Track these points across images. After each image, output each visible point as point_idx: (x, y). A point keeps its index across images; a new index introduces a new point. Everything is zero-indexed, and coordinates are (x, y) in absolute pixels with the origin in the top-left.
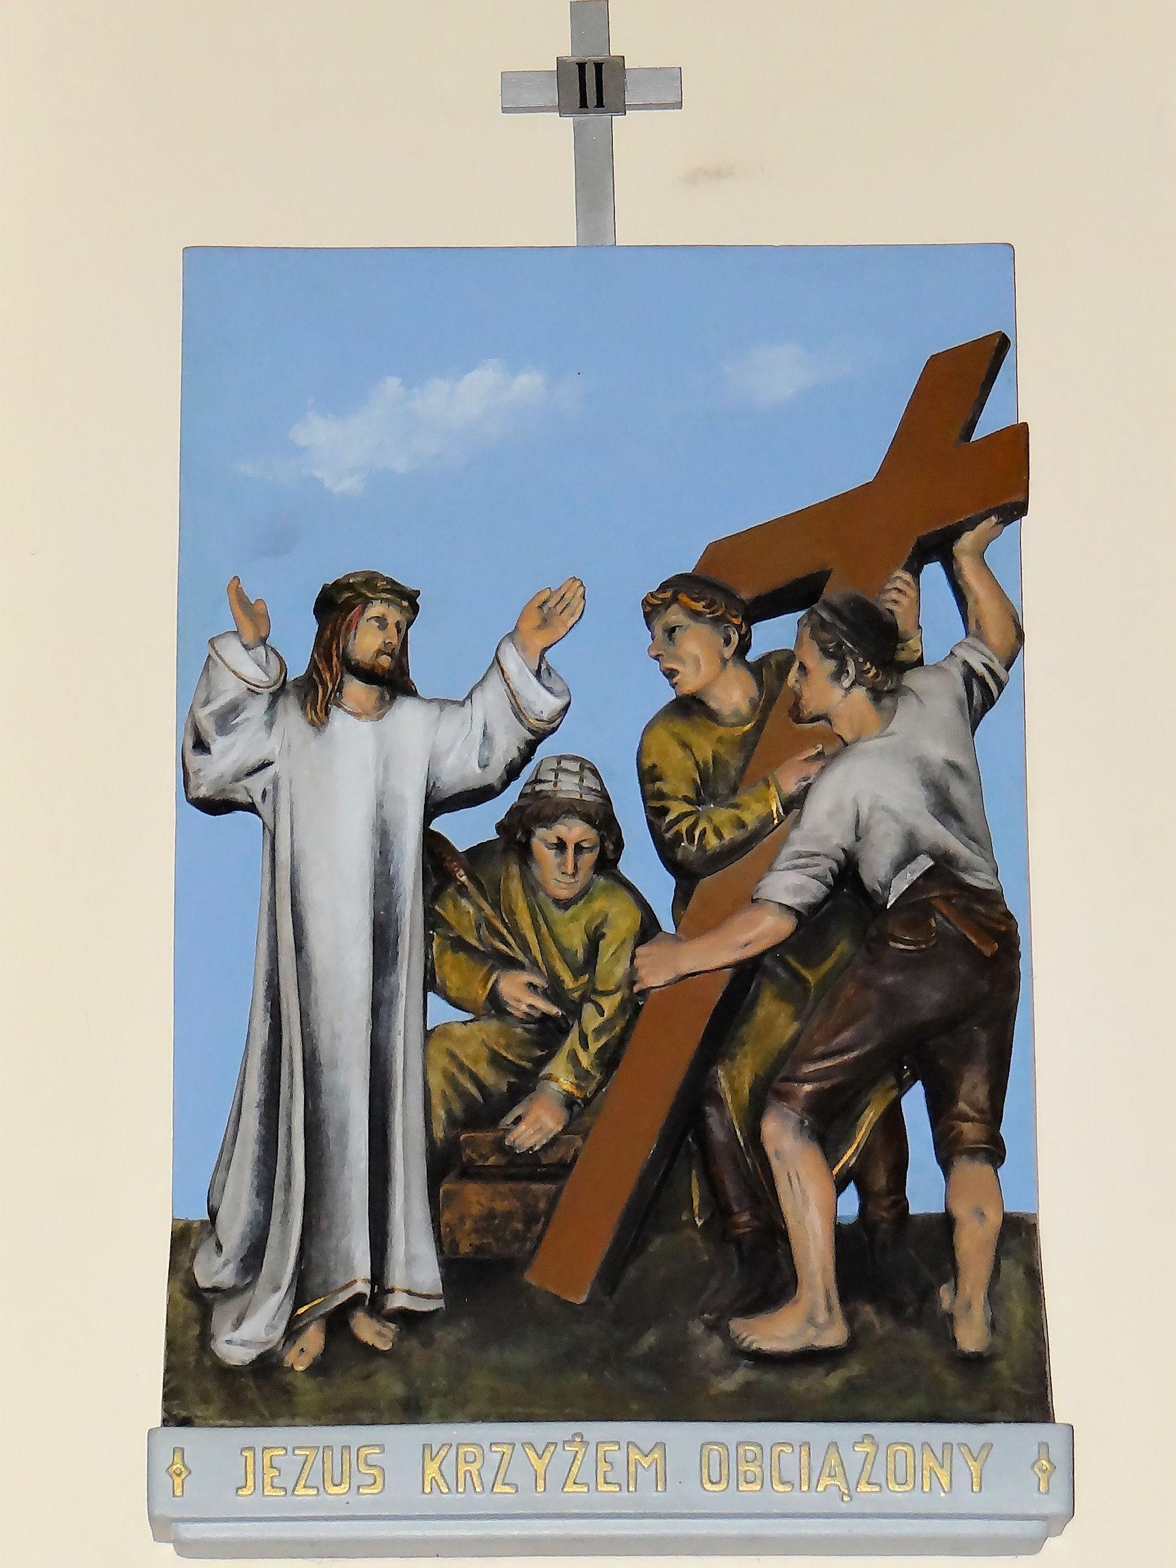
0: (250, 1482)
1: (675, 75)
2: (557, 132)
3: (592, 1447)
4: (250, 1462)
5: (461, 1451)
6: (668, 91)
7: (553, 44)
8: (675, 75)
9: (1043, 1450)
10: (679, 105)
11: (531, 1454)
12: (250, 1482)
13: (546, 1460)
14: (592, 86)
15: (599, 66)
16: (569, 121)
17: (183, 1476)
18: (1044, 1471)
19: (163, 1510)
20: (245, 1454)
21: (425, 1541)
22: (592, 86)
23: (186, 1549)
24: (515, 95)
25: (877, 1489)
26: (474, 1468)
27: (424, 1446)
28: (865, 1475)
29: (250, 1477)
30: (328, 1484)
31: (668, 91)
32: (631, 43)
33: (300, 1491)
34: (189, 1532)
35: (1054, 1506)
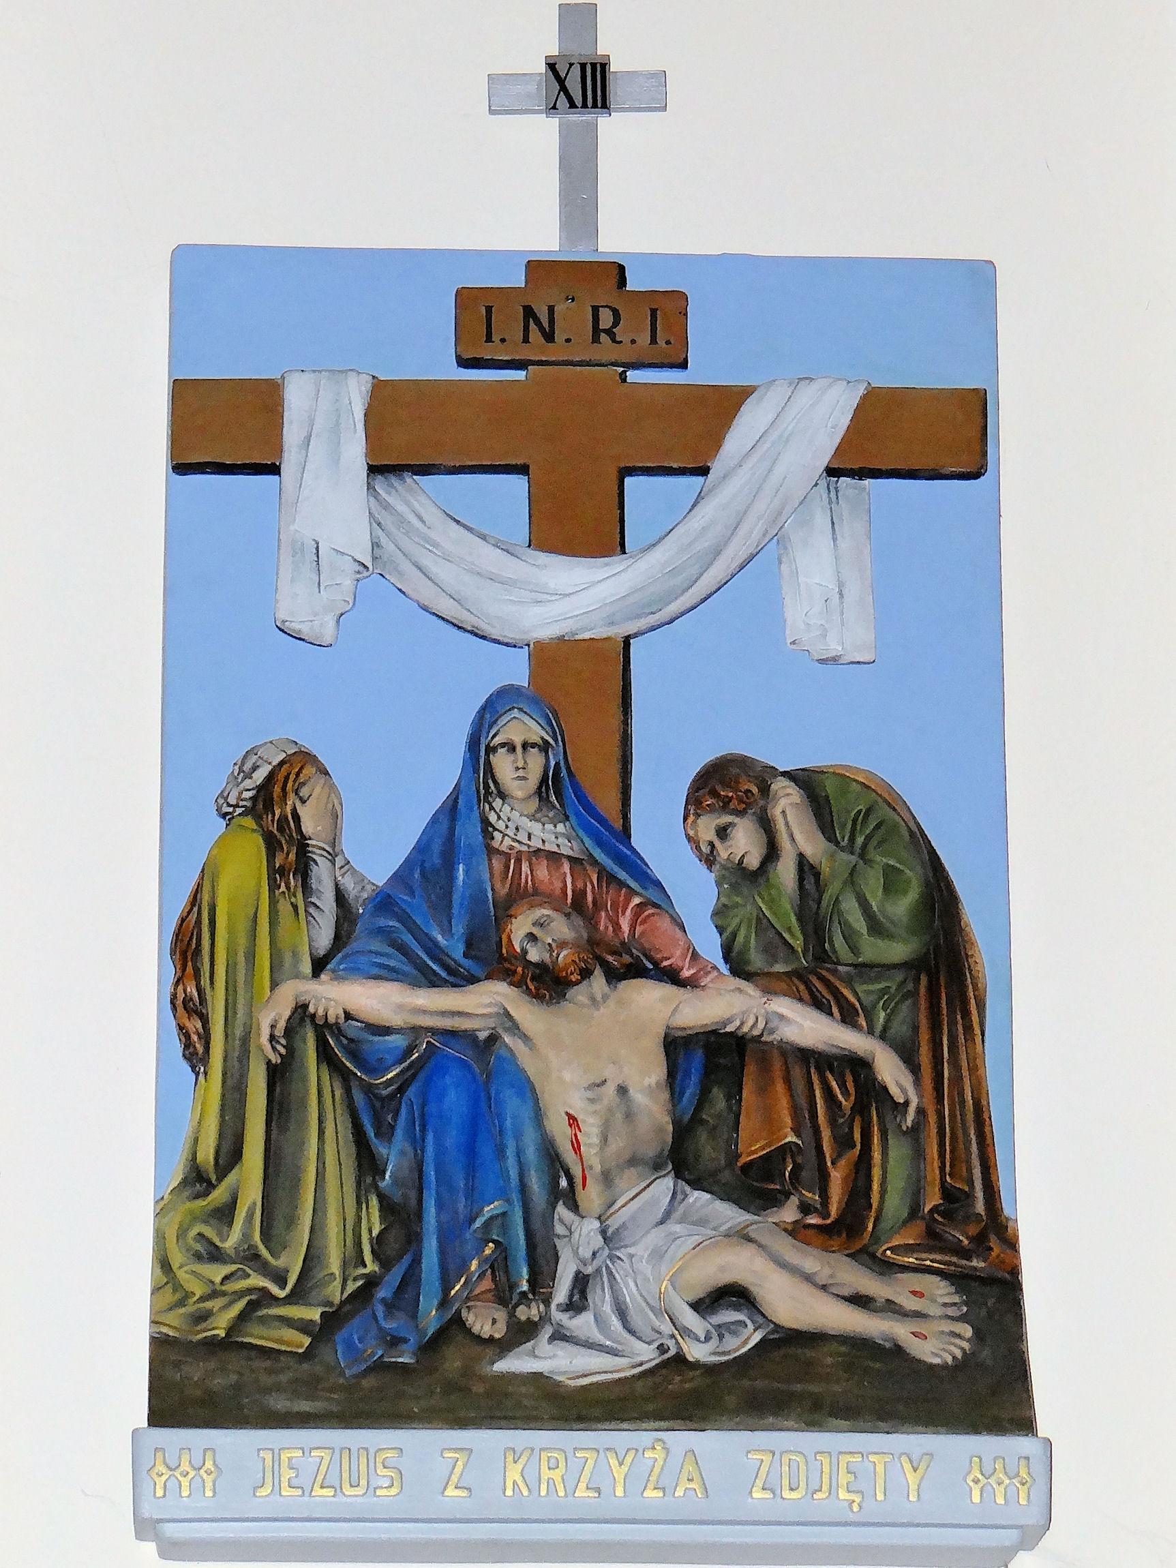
0: (825, 1488)
1: (660, 77)
2: (543, 133)
3: (777, 1456)
4: (826, 1470)
5: (785, 1459)
6: (654, 93)
7: (535, 45)
8: (660, 77)
9: (159, 1455)
10: (664, 109)
11: (907, 1466)
12: (825, 1488)
13: (921, 1471)
14: (582, 85)
15: (594, 65)
16: (554, 122)
17: (190, 1476)
18: (1023, 1484)
19: (148, 1511)
20: (262, 1454)
21: (428, 1544)
22: (582, 85)
23: (169, 1549)
24: (502, 96)
25: (299, 1492)
26: (556, 1475)
27: (205, 1450)
28: (320, 1478)
29: (269, 1475)
30: (346, 1485)
31: (654, 93)
32: (619, 47)
33: (318, 1491)
34: (170, 1530)
35: (1032, 1518)
